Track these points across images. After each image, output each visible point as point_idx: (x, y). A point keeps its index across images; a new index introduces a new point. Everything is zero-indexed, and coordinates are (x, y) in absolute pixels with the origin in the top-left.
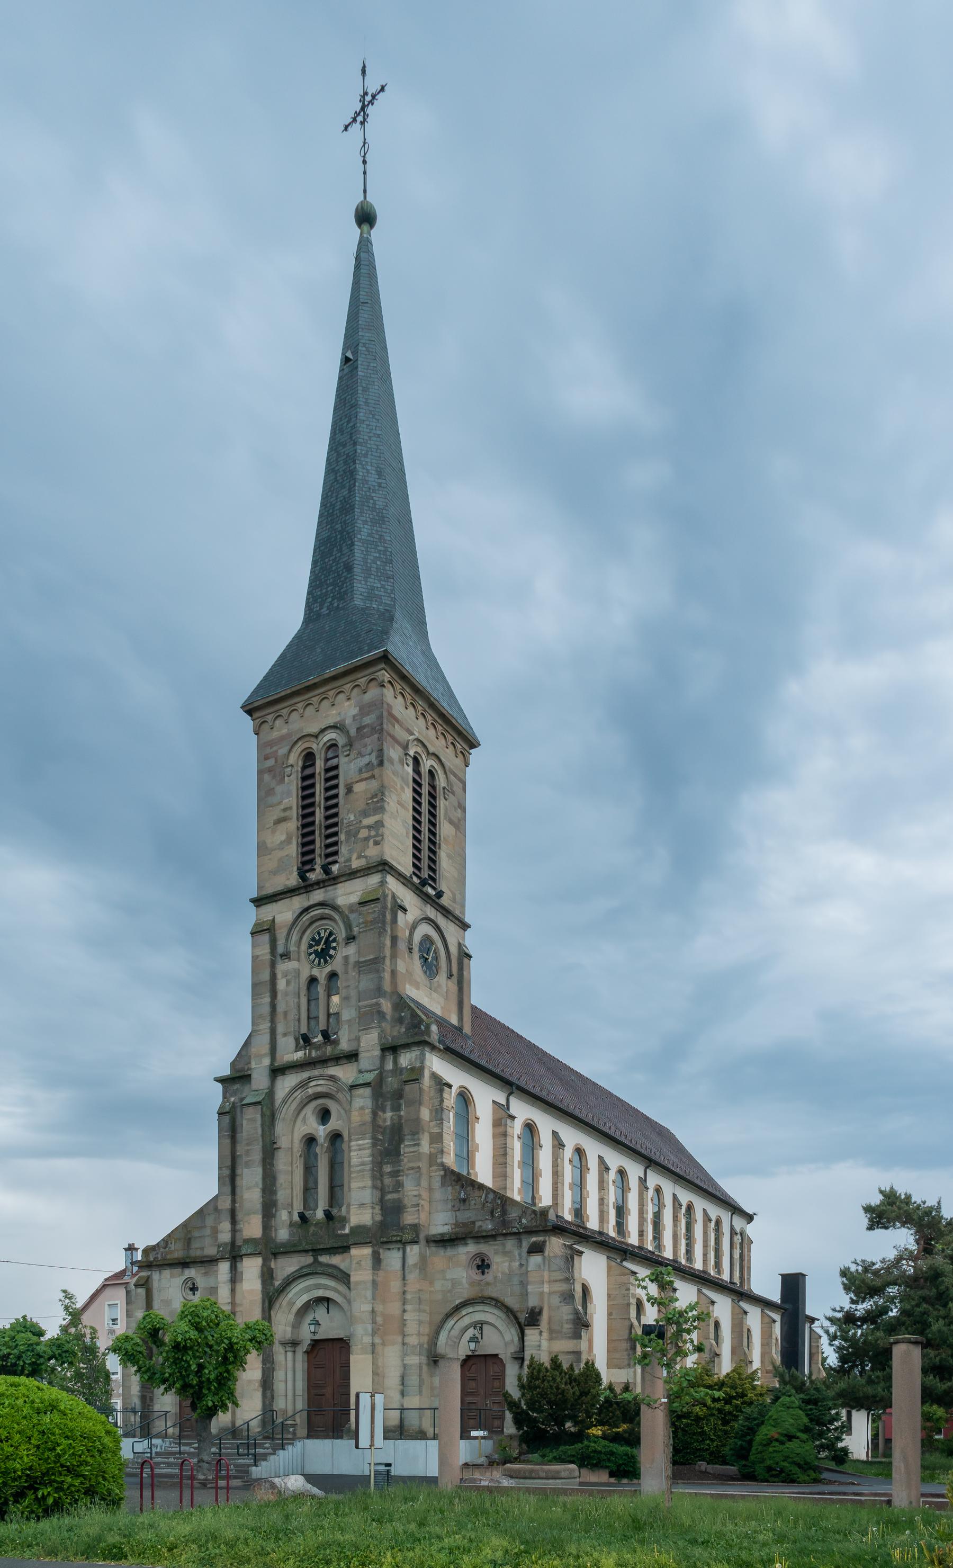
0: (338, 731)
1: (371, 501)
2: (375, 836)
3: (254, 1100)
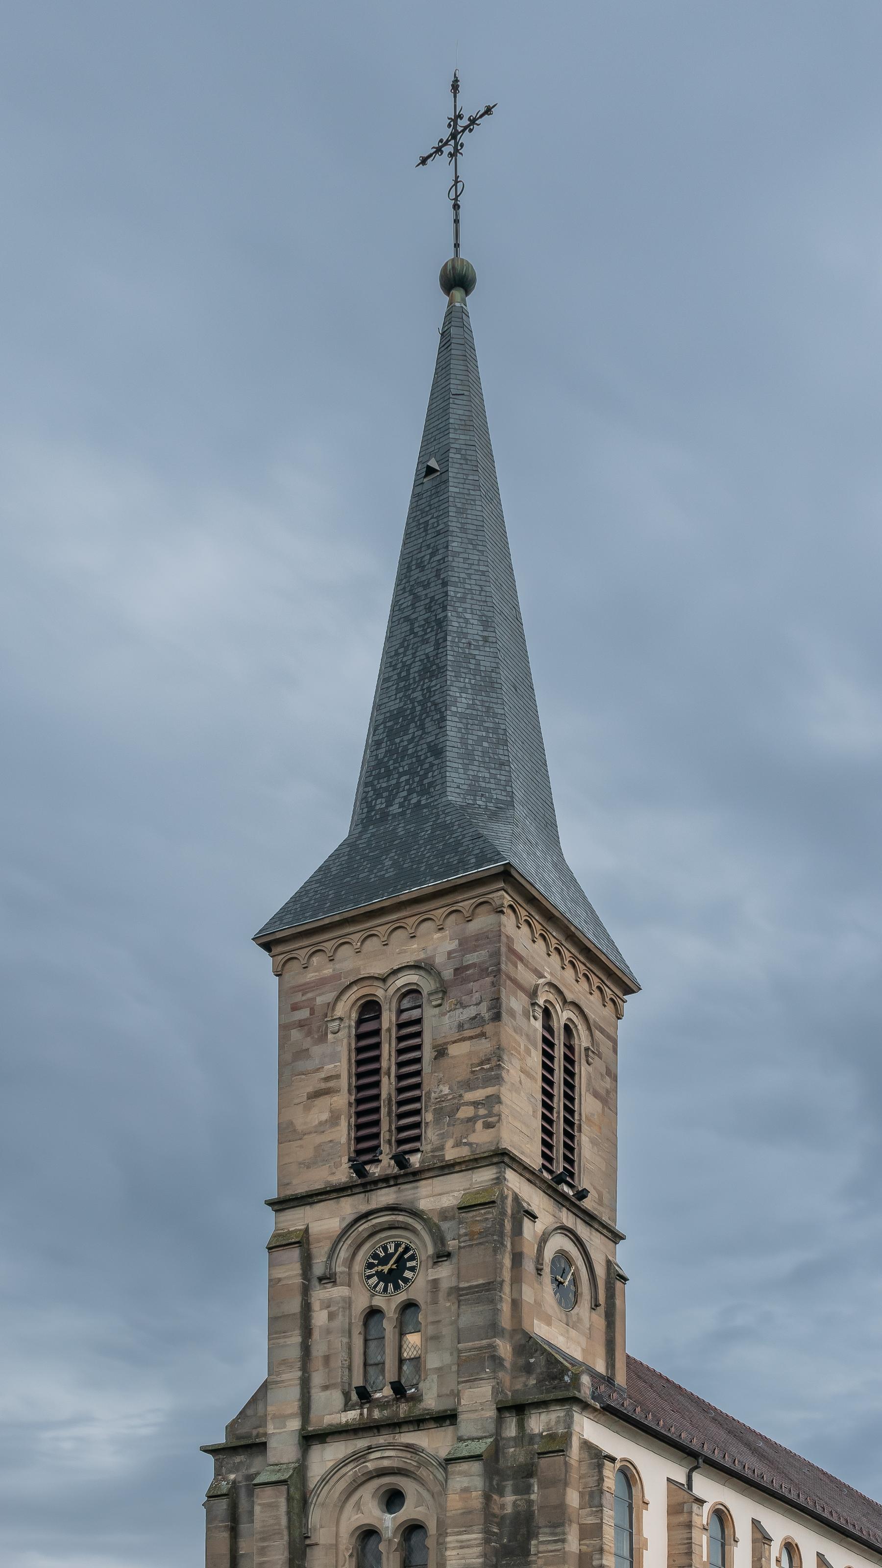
0: (422, 973)
1: (473, 661)
2: (485, 1116)
3: (274, 1478)
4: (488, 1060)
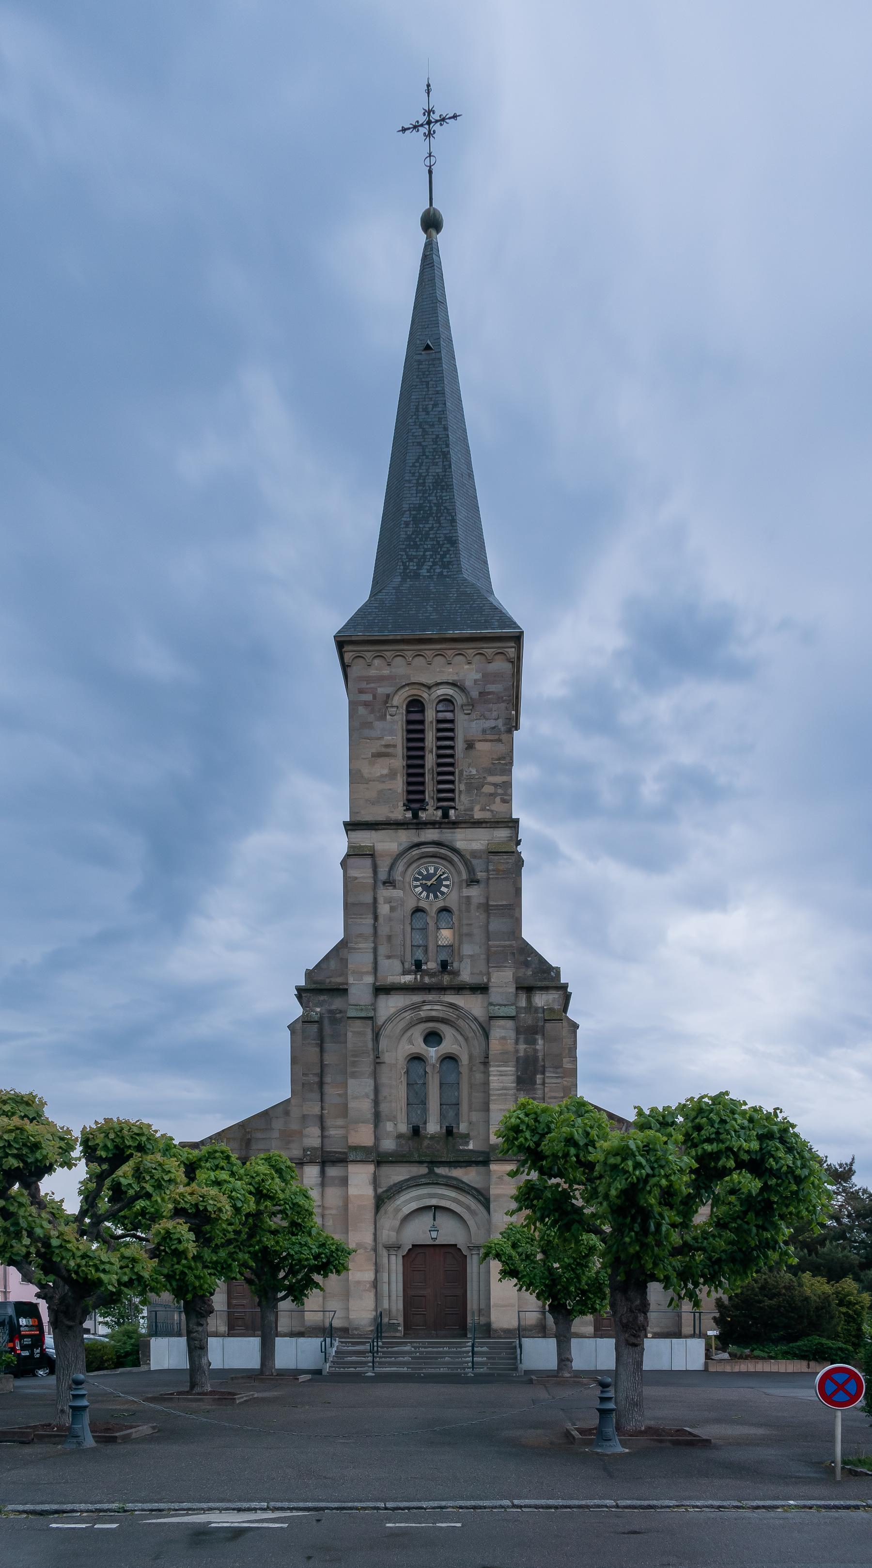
0: (456, 689)
2: (502, 794)
4: (504, 758)
